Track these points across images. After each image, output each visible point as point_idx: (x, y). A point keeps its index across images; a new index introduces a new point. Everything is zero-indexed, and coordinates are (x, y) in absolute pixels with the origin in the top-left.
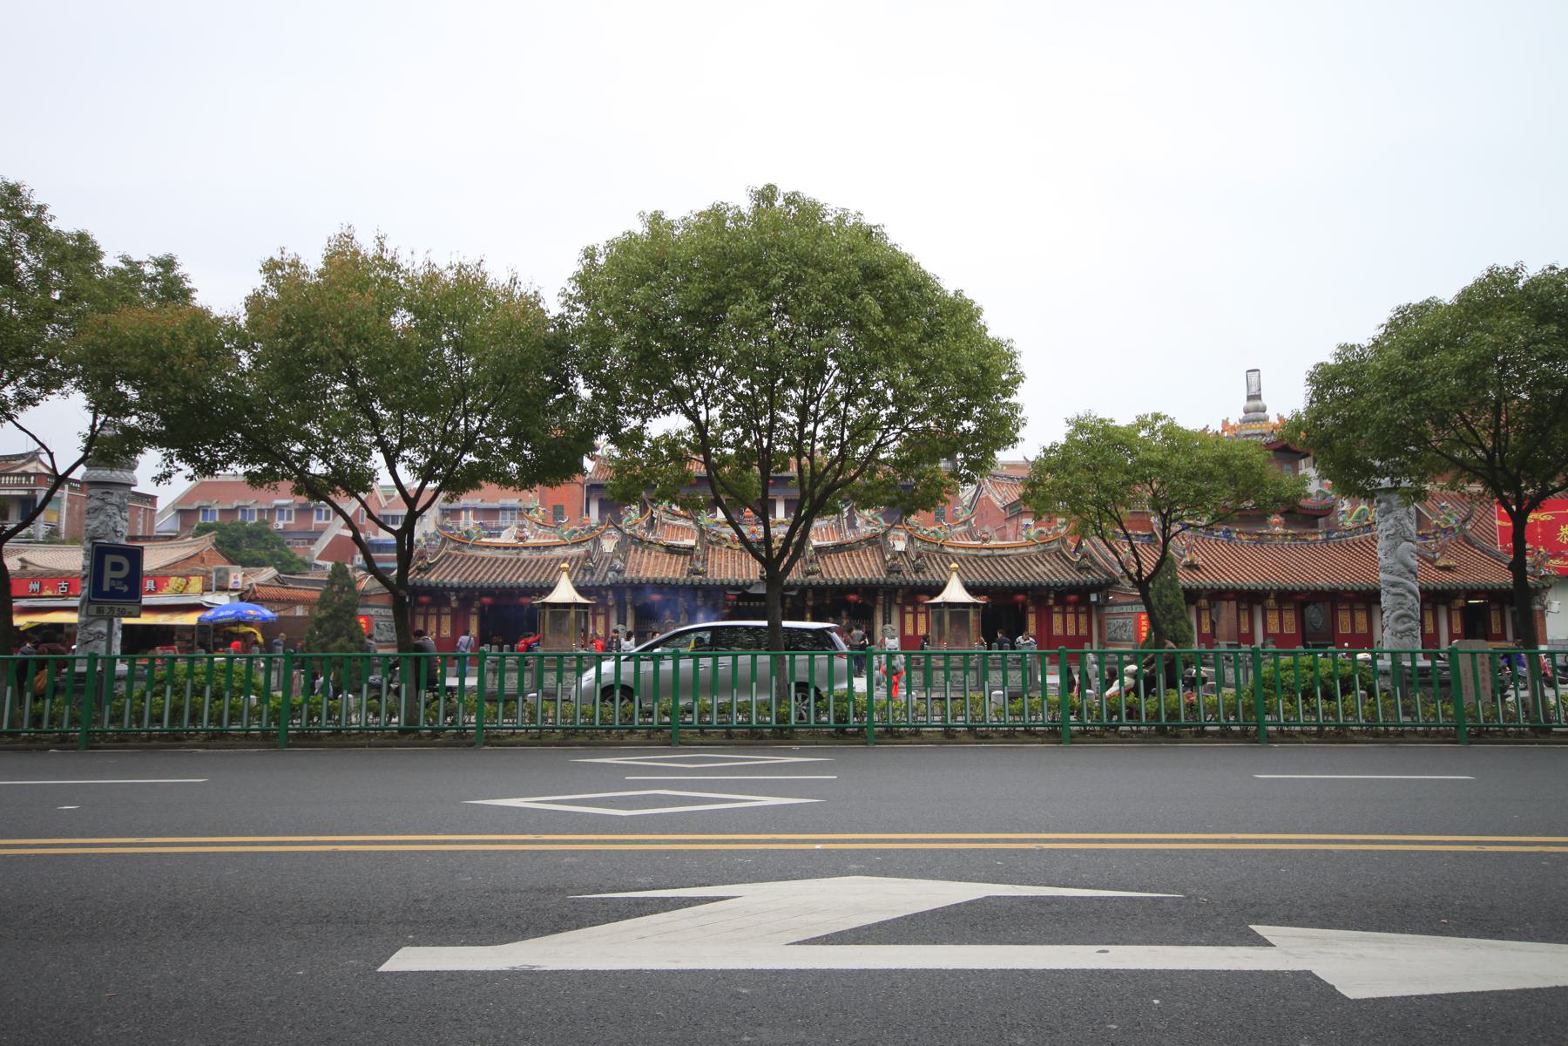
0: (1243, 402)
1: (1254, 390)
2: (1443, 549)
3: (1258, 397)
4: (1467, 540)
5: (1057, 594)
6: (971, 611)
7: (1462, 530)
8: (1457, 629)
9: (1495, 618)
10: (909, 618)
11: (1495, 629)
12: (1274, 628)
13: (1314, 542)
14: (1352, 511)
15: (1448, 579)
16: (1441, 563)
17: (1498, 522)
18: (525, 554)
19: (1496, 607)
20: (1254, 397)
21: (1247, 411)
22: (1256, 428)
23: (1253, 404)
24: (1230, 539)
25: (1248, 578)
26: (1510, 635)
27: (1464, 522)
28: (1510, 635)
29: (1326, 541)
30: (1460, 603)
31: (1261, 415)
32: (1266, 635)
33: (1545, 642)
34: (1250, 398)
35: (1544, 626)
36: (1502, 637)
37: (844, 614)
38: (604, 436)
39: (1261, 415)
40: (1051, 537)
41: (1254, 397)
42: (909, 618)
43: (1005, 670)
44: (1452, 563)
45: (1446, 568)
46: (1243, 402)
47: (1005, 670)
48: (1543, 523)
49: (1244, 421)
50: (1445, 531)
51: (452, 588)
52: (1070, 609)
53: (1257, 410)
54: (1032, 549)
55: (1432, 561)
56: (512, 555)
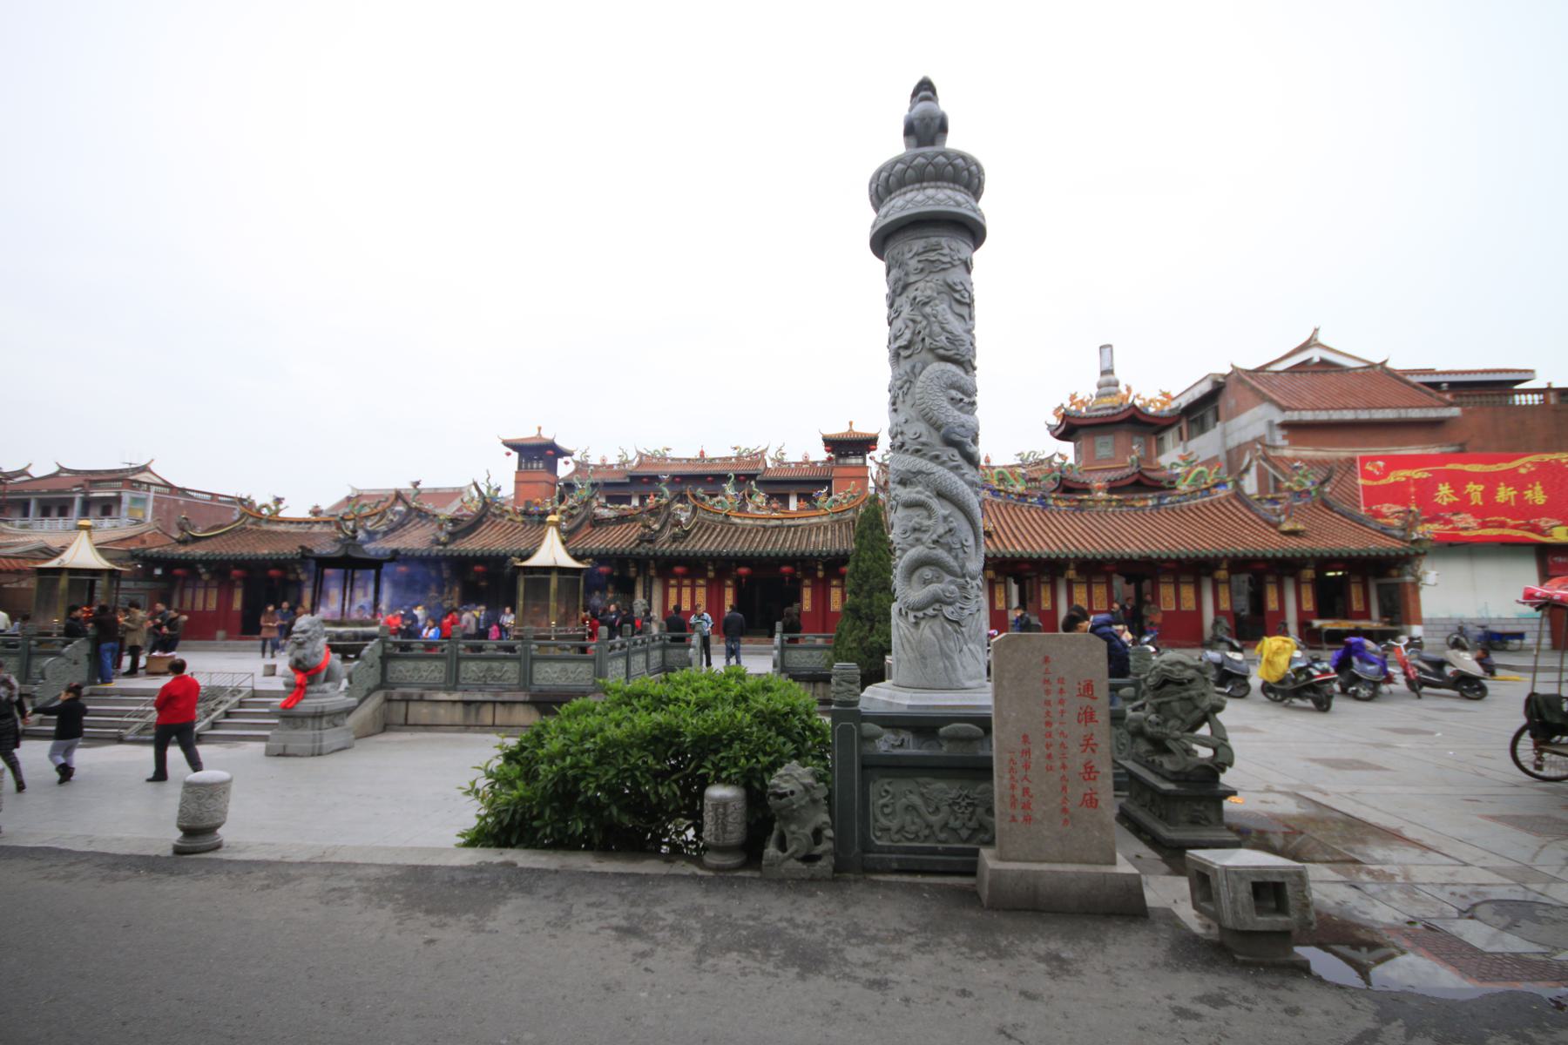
0: (1097, 377)
1: (1106, 366)
2: (1288, 511)
3: (1111, 372)
4: (1326, 504)
5: (824, 564)
6: (554, 580)
7: (1319, 492)
8: (1308, 606)
9: (1356, 593)
10: (686, 592)
11: (1357, 606)
12: (1225, 605)
13: (1143, 508)
14: (1188, 473)
15: (1293, 546)
16: (1286, 527)
17: (1361, 481)
18: (317, 528)
19: (1358, 579)
20: (1107, 372)
21: (1100, 386)
22: (1107, 402)
23: (1107, 378)
24: (1045, 506)
25: (1133, 546)
26: (1375, 612)
27: (1322, 483)
28: (1375, 612)
29: (1157, 507)
30: (1309, 574)
31: (1113, 389)
32: (1217, 611)
33: (1419, 621)
34: (1103, 373)
35: (1417, 601)
36: (1366, 615)
37: (610, 587)
38: (1071, 460)
39: (1113, 389)
40: (846, 506)
41: (1107, 372)
42: (673, 592)
43: (646, 652)
44: (1300, 527)
45: (1293, 533)
46: (1096, 377)
47: (646, 652)
48: (1417, 481)
49: (1099, 396)
50: (1299, 495)
51: (200, 561)
52: (673, 582)
53: (1109, 384)
54: (825, 519)
55: (1275, 526)
56: (302, 529)
